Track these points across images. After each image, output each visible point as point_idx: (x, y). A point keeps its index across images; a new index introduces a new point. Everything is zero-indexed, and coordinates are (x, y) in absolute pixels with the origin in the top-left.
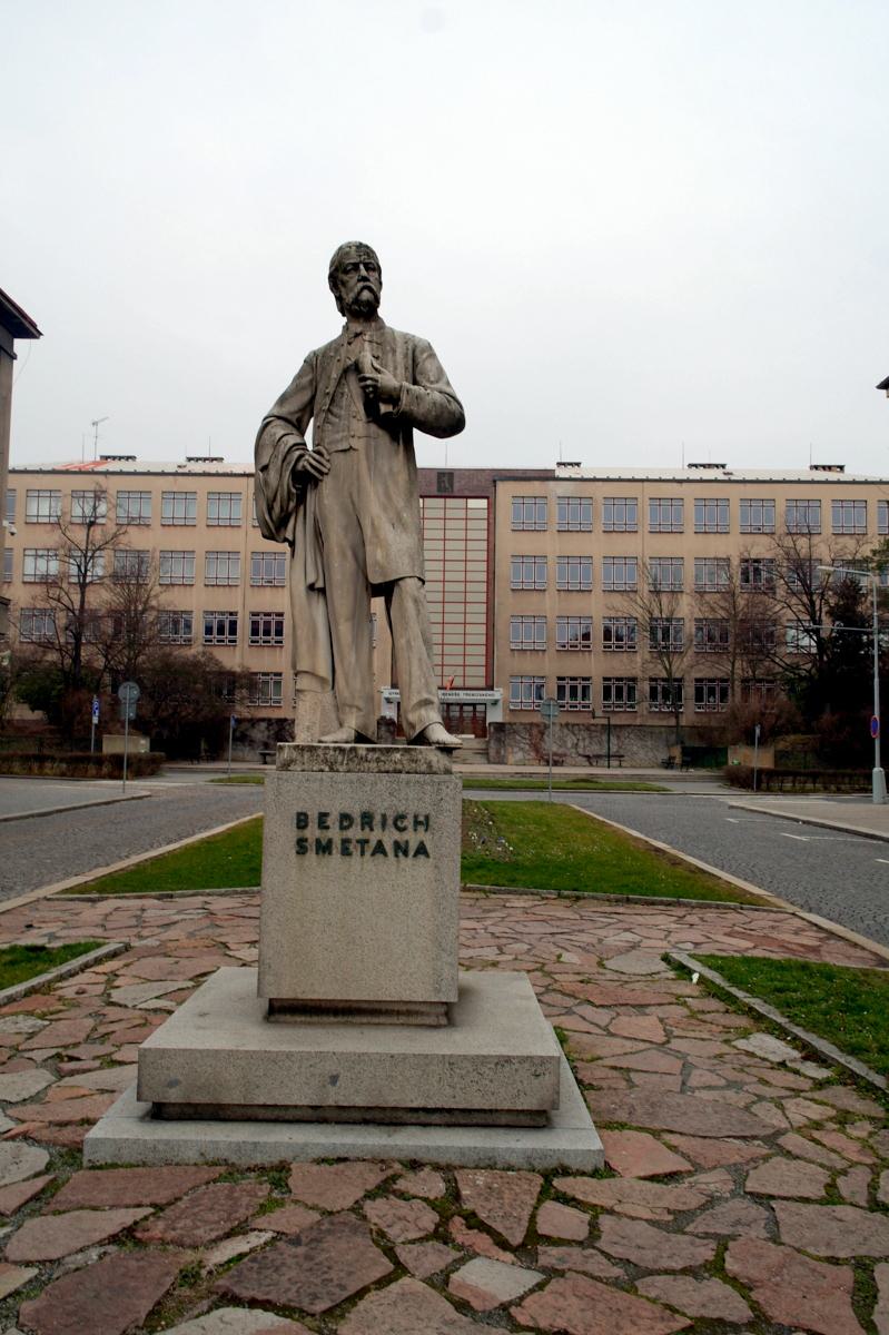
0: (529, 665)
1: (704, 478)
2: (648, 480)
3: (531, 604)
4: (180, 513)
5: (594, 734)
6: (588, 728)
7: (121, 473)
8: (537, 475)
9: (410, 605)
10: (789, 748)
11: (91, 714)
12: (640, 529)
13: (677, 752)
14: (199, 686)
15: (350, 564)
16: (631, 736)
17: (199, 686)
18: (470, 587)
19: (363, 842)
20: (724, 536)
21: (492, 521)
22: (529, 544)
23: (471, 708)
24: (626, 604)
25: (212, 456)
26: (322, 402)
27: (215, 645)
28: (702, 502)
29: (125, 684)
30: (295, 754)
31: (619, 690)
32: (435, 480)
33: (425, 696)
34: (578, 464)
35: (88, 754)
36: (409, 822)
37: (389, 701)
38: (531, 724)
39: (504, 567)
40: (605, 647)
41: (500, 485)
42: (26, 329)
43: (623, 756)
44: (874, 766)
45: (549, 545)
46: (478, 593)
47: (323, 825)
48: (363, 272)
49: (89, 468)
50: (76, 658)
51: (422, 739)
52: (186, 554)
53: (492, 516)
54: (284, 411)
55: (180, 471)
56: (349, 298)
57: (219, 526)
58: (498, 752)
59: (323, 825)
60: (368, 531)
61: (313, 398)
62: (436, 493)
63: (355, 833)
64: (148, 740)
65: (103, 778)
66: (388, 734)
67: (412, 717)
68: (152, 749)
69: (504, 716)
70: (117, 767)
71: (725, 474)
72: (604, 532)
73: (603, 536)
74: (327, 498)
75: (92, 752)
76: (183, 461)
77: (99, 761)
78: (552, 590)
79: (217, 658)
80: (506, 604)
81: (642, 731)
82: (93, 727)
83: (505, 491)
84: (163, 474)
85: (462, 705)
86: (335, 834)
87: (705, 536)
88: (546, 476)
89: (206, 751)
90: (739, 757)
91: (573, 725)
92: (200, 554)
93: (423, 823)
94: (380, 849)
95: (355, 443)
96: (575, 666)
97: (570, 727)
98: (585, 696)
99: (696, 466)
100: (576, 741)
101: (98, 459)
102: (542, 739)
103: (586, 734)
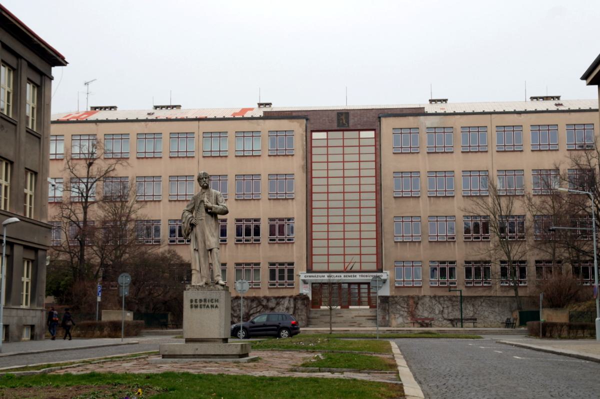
0: (408, 253)
1: (539, 109)
2: (495, 113)
3: (408, 208)
4: (150, 149)
5: (456, 303)
6: (450, 299)
7: (107, 121)
8: (410, 112)
9: (215, 254)
10: (586, 310)
11: (97, 295)
12: (489, 149)
13: (516, 314)
14: (167, 275)
15: (203, 245)
16: (484, 304)
17: (167, 275)
18: (363, 196)
19: (204, 305)
20: (554, 153)
21: (378, 147)
22: (406, 163)
23: (366, 286)
24: (474, 207)
25: (173, 104)
26: (196, 208)
27: (177, 245)
28: (536, 128)
29: (122, 275)
30: (190, 287)
31: (478, 270)
32: (335, 119)
33: (218, 274)
34: (445, 101)
35: (94, 322)
36: (214, 301)
37: (305, 282)
38: (408, 297)
39: (388, 181)
40: (465, 238)
41: (383, 120)
42: (57, 60)
43: (476, 319)
44: (596, 317)
45: (421, 163)
46: (370, 200)
47: (196, 302)
48: (205, 180)
49: (84, 118)
50: (81, 258)
51: (217, 283)
52: (155, 179)
53: (378, 143)
54: (188, 209)
55: (150, 118)
56: (202, 185)
57: (178, 157)
58: (384, 318)
59: (196, 302)
60: (206, 238)
61: (194, 206)
62: (336, 128)
63: (203, 303)
64: (132, 313)
65: (105, 337)
66: (303, 306)
67: (216, 279)
68: (134, 318)
69: (391, 291)
70: (115, 329)
71: (556, 105)
72: (462, 152)
73: (461, 155)
74: (197, 230)
75: (97, 321)
76: (152, 110)
77: (101, 327)
78: (424, 196)
79: (179, 254)
80: (391, 209)
81: (492, 301)
82: (98, 303)
83: (387, 125)
84: (137, 121)
85: (359, 284)
86: (198, 303)
87: (539, 153)
88: (418, 112)
89: (172, 321)
90: (547, 315)
91: (440, 297)
92: (165, 179)
93: (217, 301)
94: (208, 306)
95: (203, 218)
96: (445, 253)
97: (437, 299)
98: (451, 276)
99: (537, 98)
100: (442, 309)
101: (89, 109)
102: (416, 307)
103: (448, 303)
